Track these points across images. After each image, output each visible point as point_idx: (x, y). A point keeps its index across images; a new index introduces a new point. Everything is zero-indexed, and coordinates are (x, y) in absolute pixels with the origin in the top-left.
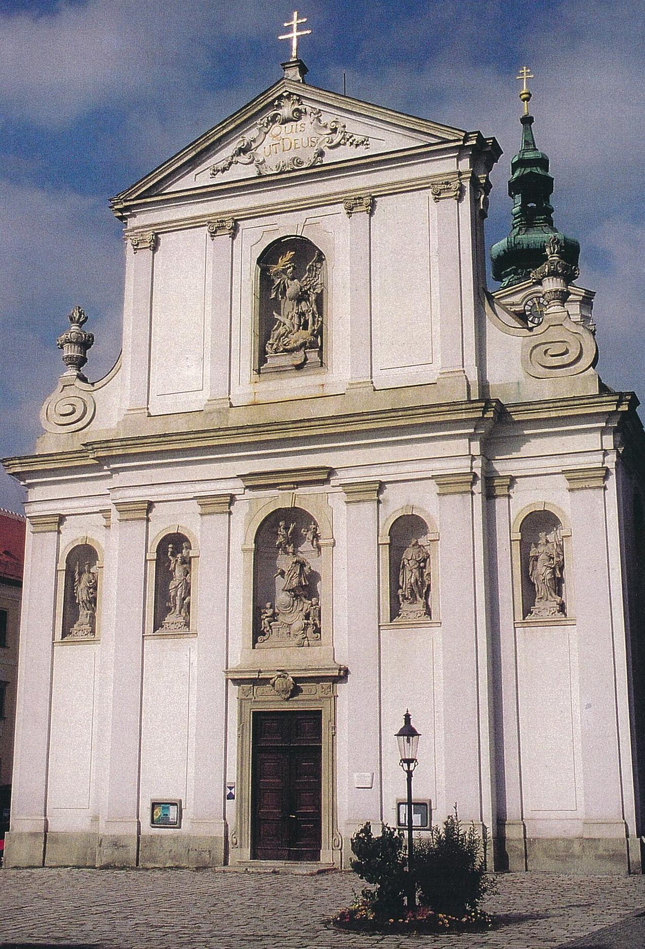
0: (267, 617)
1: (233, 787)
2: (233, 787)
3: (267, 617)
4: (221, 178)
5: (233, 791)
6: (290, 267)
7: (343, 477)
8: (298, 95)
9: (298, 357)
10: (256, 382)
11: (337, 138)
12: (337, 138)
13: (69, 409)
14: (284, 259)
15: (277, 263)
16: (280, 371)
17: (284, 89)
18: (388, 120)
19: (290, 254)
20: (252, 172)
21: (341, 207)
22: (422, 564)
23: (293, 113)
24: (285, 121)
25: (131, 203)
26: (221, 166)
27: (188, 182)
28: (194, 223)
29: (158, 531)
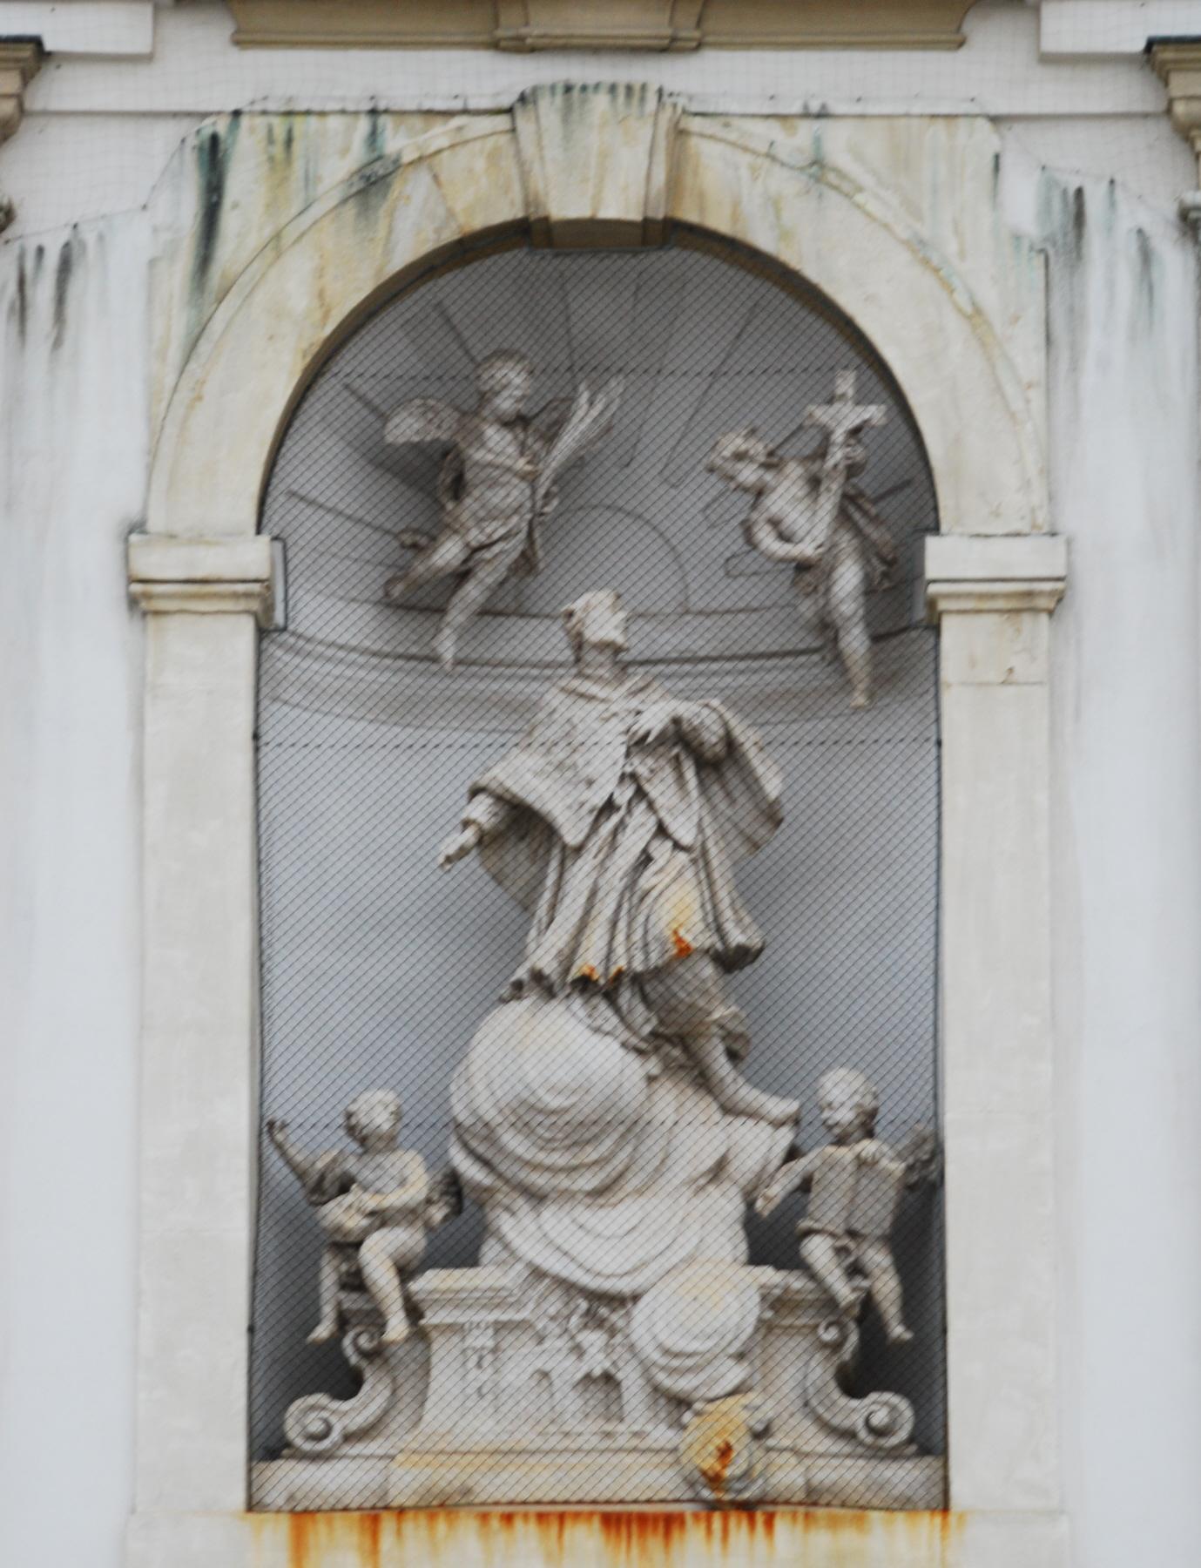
0: (381, 1218)
3: (381, 1218)
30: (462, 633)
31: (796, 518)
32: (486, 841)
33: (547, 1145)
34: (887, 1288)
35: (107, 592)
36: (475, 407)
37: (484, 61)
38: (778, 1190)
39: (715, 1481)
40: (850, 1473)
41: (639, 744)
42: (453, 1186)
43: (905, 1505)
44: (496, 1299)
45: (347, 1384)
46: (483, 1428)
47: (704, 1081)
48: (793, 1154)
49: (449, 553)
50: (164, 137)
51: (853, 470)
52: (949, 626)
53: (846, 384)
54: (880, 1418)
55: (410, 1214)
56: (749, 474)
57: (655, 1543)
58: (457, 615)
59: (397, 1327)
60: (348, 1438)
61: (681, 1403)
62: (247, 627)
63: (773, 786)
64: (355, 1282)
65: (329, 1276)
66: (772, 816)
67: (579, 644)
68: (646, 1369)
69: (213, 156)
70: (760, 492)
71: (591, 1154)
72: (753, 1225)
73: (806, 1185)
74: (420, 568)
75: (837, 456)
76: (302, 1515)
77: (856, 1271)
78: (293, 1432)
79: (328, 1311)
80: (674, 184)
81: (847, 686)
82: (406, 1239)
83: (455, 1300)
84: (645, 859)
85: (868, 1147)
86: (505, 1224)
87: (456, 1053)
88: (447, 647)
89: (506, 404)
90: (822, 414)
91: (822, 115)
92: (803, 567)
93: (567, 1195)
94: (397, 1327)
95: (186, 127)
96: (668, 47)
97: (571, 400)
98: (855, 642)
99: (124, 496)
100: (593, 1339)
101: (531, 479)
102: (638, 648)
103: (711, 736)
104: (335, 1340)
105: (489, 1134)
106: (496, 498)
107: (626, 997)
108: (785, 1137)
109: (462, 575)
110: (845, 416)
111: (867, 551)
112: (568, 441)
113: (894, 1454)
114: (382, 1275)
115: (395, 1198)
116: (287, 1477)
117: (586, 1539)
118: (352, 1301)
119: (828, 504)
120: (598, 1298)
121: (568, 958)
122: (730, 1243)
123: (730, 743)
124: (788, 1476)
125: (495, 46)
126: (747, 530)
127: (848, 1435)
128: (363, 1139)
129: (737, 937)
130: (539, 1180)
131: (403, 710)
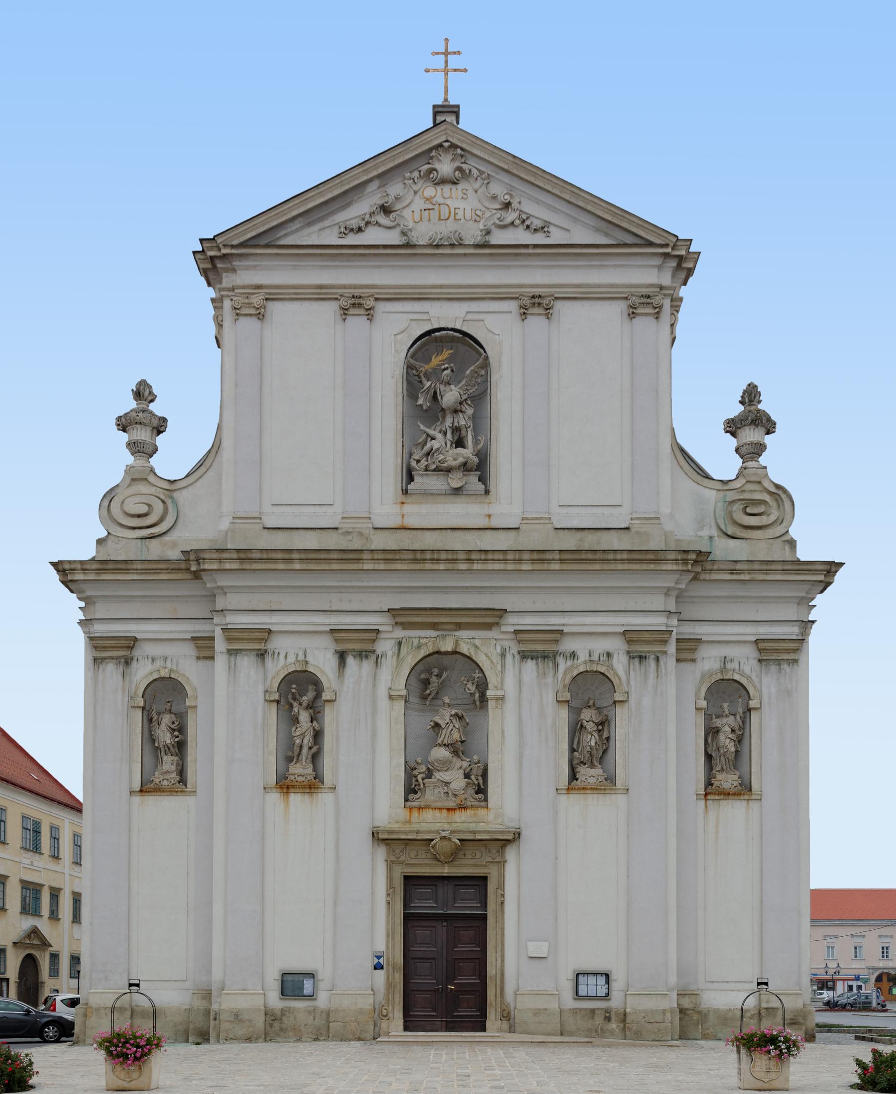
0: (420, 773)
1: (381, 956)
2: (381, 956)
3: (420, 773)
4: (352, 239)
5: (381, 961)
6: (446, 369)
7: (512, 622)
8: (462, 149)
9: (456, 481)
10: (403, 503)
11: (511, 216)
12: (511, 216)
13: (144, 509)
14: (440, 358)
15: (429, 360)
16: (427, 495)
17: (444, 138)
18: (581, 204)
19: (446, 354)
20: (393, 238)
21: (513, 306)
22: (600, 727)
23: (455, 173)
24: (443, 181)
25: (234, 251)
26: (354, 224)
27: (312, 236)
28: (321, 294)
29: (277, 668)
30: (430, 701)
31: (471, 688)
32: (433, 727)
33: (440, 764)
34: (481, 782)
35: (387, 696)
36: (431, 674)
37: (432, 631)
38: (468, 770)
39: (460, 805)
40: (477, 803)
41: (451, 716)
42: (428, 769)
43: (483, 807)
44: (434, 783)
45: (416, 793)
46: (432, 798)
47: (459, 757)
48: (470, 765)
49: (428, 692)
50: (393, 641)
51: (478, 682)
52: (489, 701)
53: (477, 671)
54: (480, 797)
55: (423, 773)
56: (465, 682)
57: (453, 812)
58: (429, 699)
59: (422, 786)
60: (416, 799)
61: (456, 795)
62: (404, 701)
63: (468, 721)
64: (417, 781)
65: (414, 780)
66: (468, 724)
67: (444, 703)
68: (452, 791)
69: (400, 644)
70: (466, 684)
71: (445, 765)
72: (465, 774)
73: (471, 769)
74: (424, 693)
75: (476, 680)
76: (411, 808)
77: (477, 779)
78: (409, 798)
79: (414, 784)
80: (456, 647)
81: (477, 708)
82: (423, 775)
83: (429, 783)
84: (452, 729)
85: (479, 765)
86: (435, 774)
87: (429, 752)
88: (428, 703)
89: (435, 673)
90: (474, 675)
91: (474, 638)
92: (471, 694)
93: (442, 771)
94: (422, 786)
95: (395, 640)
96: (456, 630)
97: (443, 672)
98: (478, 703)
99: (389, 685)
100: (445, 788)
101: (438, 683)
102: (451, 703)
103: (460, 715)
104: (414, 787)
105: (433, 763)
106: (434, 685)
107: (449, 746)
108: (469, 763)
109: (430, 694)
110: (478, 675)
111: (479, 692)
112: (443, 678)
113: (482, 801)
114: (420, 780)
115: (421, 771)
116: (409, 804)
117: (445, 811)
118: (417, 783)
119: (475, 686)
120: (446, 783)
121: (443, 742)
122: (462, 776)
123: (462, 715)
124: (469, 804)
125: (434, 630)
126: (465, 689)
127: (476, 799)
128: (418, 764)
129: (463, 739)
130: (439, 769)
131: (422, 711)
